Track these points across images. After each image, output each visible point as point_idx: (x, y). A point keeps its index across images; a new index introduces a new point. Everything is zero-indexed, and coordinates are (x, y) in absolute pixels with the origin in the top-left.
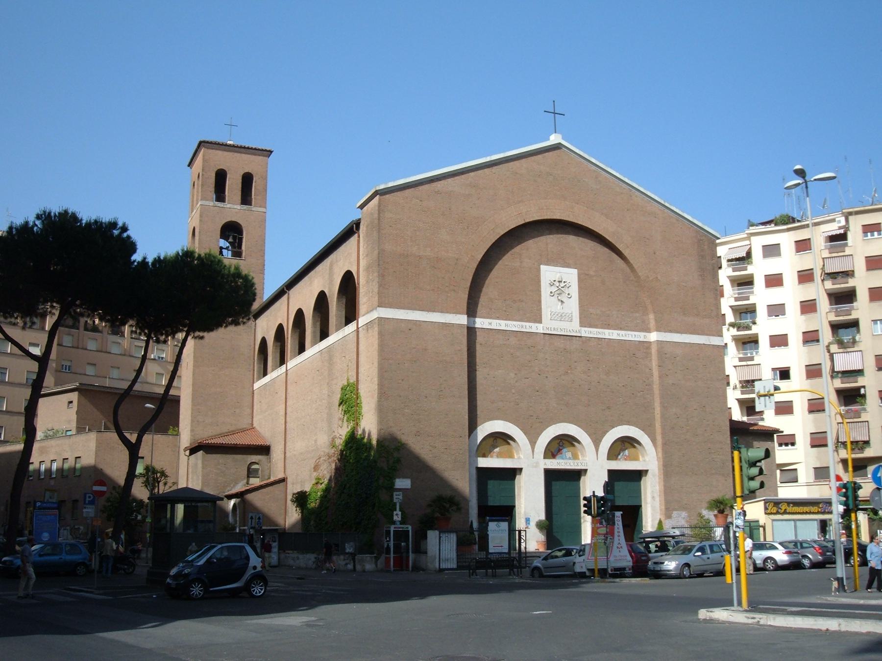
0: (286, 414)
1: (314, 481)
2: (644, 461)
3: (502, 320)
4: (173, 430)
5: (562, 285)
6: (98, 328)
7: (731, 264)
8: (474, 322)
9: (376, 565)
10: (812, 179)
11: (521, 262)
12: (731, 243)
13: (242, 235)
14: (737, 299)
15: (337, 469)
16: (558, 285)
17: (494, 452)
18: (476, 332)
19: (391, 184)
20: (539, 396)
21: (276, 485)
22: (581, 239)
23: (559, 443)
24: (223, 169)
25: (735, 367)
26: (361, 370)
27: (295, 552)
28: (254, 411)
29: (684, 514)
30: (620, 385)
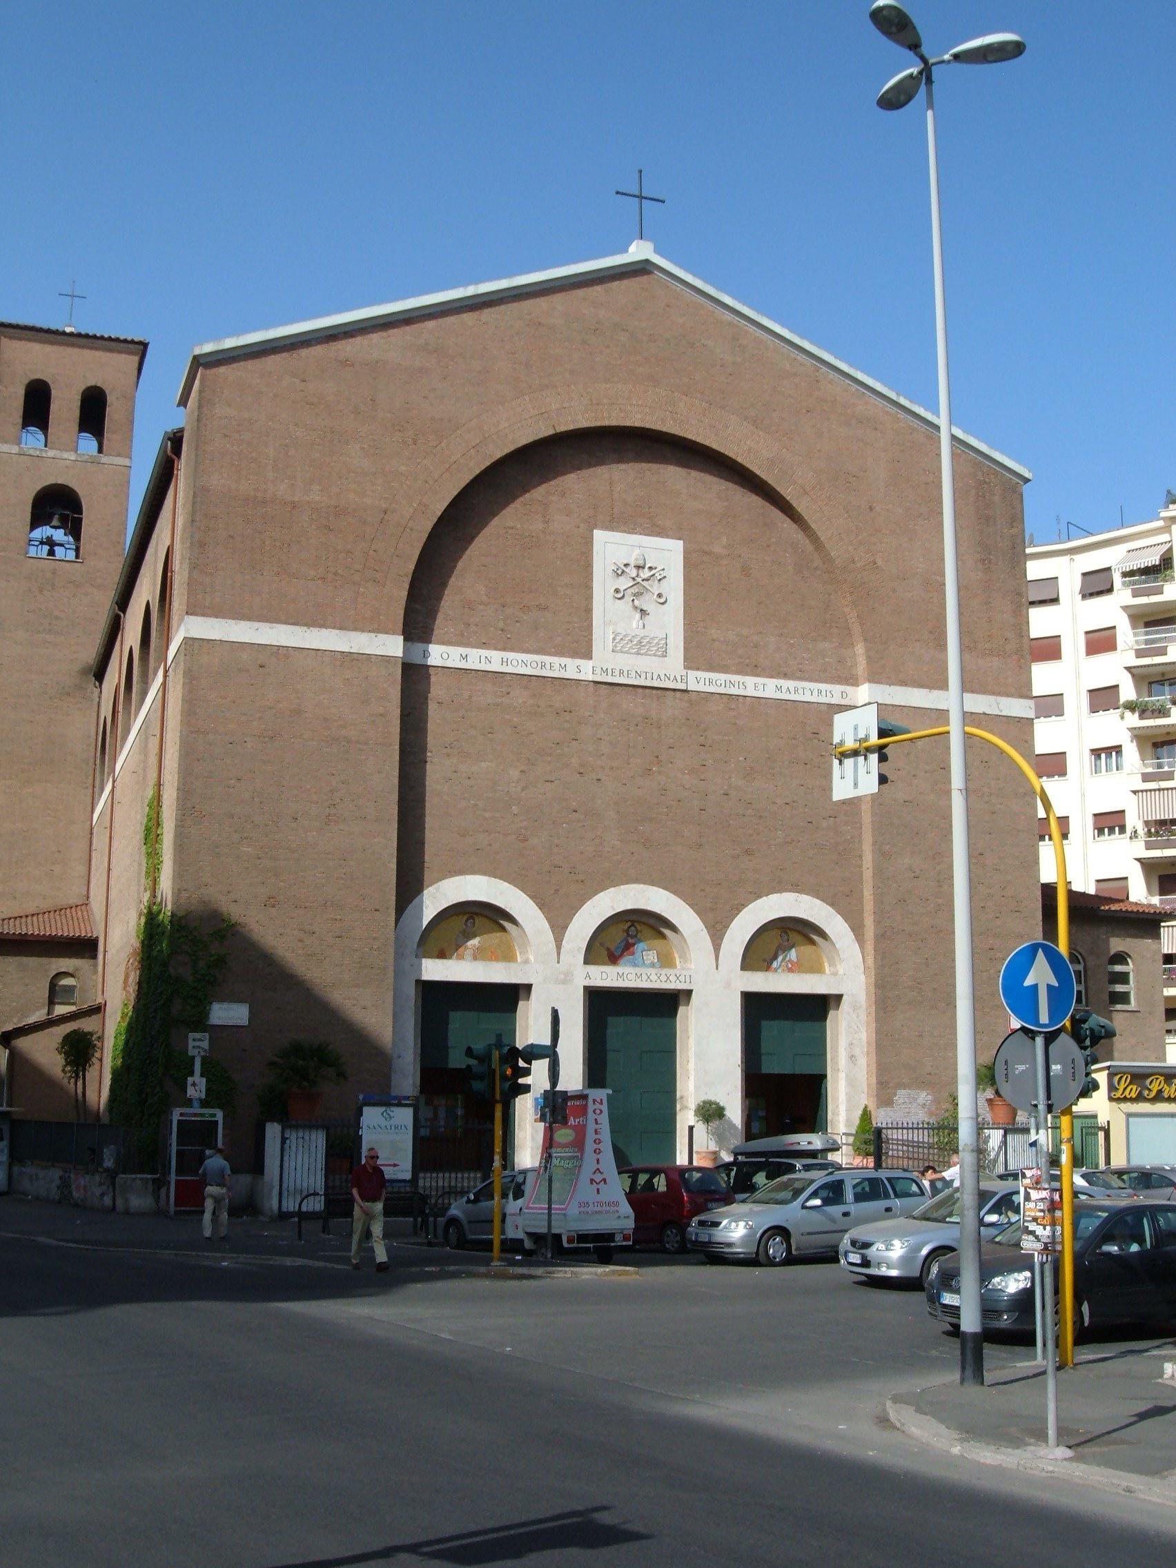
2: (835, 974)
3: (496, 649)
5: (645, 574)
7: (1130, 581)
8: (426, 654)
9: (157, 1201)
10: (946, 57)
11: (547, 522)
12: (1133, 540)
13: (82, 514)
14: (1140, 654)
16: (634, 576)
17: (466, 948)
18: (428, 676)
19: (229, 343)
20: (579, 821)
22: (694, 473)
23: (627, 931)
25: (1135, 792)
29: (924, 1096)
30: (778, 801)
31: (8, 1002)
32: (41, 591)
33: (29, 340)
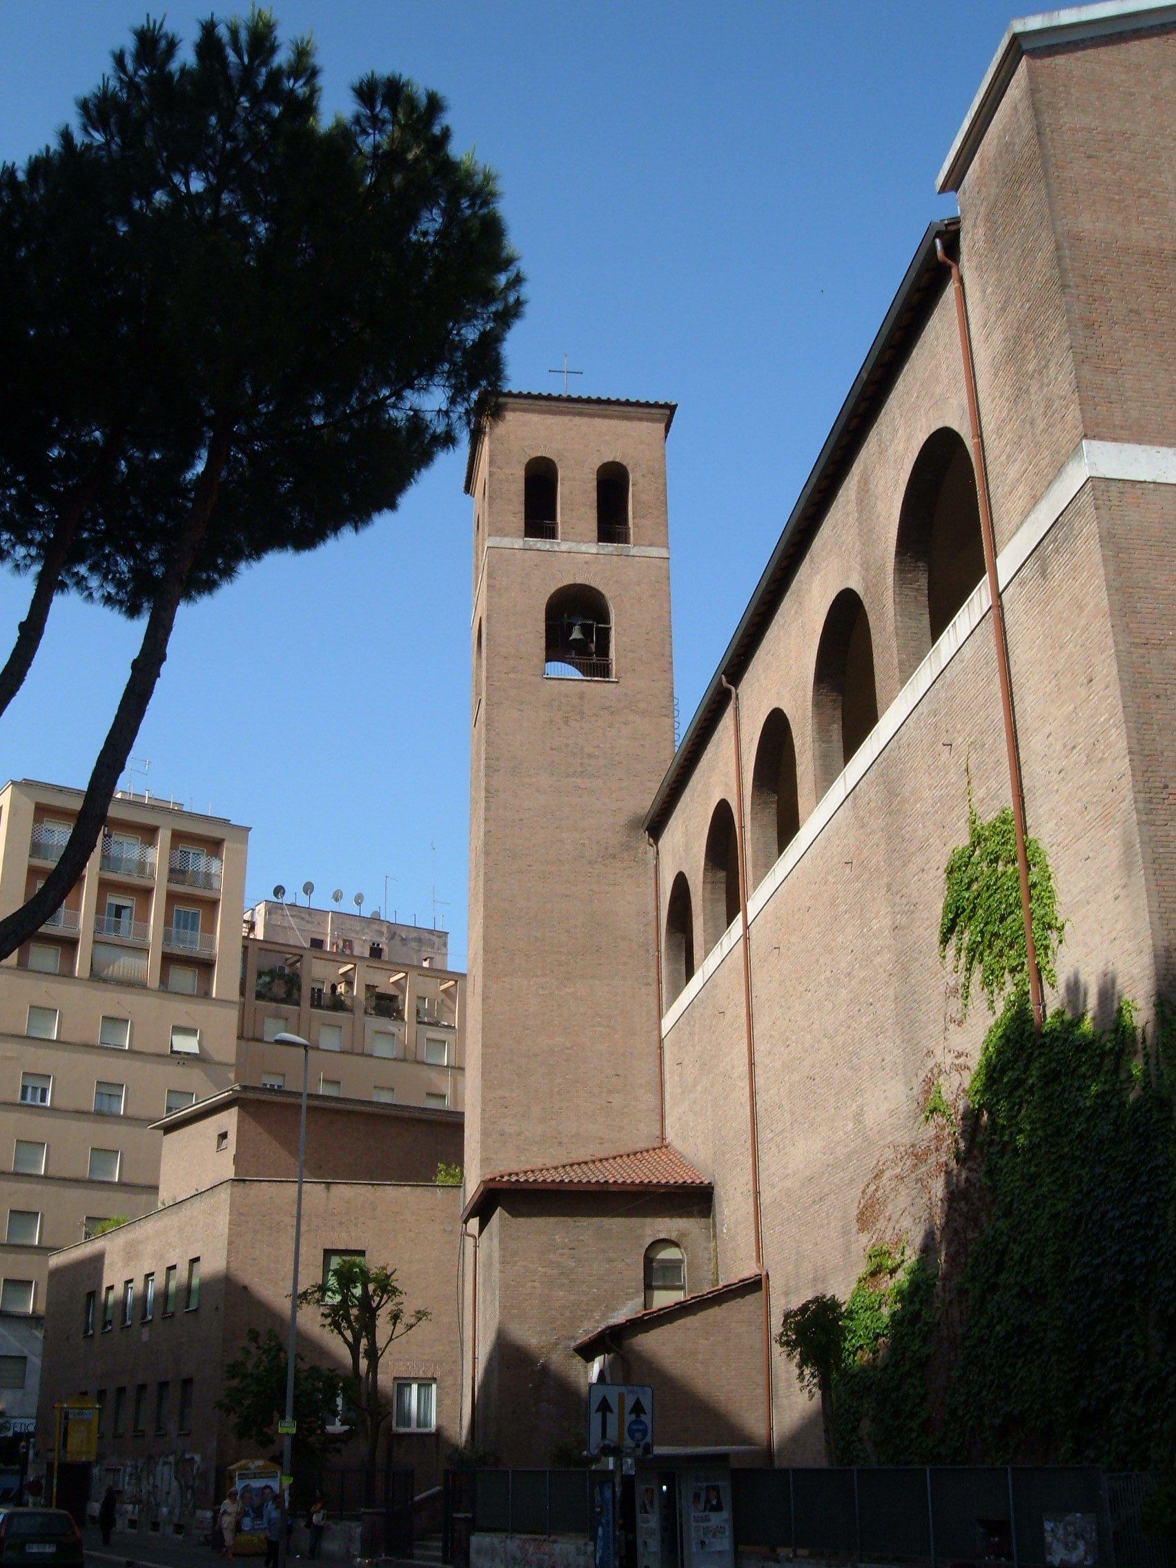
0: (752, 1064)
1: (863, 1268)
4: (447, 1174)
6: (343, 1002)
13: (608, 622)
15: (954, 1197)
19: (1067, 17)
21: (732, 1303)
24: (544, 458)
26: (1031, 746)
27: (802, 1552)
28: (667, 1096)
31: (584, 1287)
32: (566, 722)
33: (525, 411)
